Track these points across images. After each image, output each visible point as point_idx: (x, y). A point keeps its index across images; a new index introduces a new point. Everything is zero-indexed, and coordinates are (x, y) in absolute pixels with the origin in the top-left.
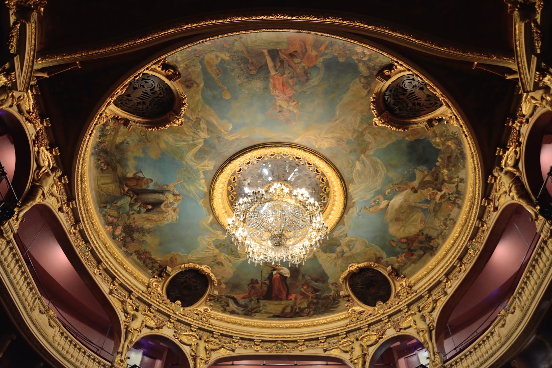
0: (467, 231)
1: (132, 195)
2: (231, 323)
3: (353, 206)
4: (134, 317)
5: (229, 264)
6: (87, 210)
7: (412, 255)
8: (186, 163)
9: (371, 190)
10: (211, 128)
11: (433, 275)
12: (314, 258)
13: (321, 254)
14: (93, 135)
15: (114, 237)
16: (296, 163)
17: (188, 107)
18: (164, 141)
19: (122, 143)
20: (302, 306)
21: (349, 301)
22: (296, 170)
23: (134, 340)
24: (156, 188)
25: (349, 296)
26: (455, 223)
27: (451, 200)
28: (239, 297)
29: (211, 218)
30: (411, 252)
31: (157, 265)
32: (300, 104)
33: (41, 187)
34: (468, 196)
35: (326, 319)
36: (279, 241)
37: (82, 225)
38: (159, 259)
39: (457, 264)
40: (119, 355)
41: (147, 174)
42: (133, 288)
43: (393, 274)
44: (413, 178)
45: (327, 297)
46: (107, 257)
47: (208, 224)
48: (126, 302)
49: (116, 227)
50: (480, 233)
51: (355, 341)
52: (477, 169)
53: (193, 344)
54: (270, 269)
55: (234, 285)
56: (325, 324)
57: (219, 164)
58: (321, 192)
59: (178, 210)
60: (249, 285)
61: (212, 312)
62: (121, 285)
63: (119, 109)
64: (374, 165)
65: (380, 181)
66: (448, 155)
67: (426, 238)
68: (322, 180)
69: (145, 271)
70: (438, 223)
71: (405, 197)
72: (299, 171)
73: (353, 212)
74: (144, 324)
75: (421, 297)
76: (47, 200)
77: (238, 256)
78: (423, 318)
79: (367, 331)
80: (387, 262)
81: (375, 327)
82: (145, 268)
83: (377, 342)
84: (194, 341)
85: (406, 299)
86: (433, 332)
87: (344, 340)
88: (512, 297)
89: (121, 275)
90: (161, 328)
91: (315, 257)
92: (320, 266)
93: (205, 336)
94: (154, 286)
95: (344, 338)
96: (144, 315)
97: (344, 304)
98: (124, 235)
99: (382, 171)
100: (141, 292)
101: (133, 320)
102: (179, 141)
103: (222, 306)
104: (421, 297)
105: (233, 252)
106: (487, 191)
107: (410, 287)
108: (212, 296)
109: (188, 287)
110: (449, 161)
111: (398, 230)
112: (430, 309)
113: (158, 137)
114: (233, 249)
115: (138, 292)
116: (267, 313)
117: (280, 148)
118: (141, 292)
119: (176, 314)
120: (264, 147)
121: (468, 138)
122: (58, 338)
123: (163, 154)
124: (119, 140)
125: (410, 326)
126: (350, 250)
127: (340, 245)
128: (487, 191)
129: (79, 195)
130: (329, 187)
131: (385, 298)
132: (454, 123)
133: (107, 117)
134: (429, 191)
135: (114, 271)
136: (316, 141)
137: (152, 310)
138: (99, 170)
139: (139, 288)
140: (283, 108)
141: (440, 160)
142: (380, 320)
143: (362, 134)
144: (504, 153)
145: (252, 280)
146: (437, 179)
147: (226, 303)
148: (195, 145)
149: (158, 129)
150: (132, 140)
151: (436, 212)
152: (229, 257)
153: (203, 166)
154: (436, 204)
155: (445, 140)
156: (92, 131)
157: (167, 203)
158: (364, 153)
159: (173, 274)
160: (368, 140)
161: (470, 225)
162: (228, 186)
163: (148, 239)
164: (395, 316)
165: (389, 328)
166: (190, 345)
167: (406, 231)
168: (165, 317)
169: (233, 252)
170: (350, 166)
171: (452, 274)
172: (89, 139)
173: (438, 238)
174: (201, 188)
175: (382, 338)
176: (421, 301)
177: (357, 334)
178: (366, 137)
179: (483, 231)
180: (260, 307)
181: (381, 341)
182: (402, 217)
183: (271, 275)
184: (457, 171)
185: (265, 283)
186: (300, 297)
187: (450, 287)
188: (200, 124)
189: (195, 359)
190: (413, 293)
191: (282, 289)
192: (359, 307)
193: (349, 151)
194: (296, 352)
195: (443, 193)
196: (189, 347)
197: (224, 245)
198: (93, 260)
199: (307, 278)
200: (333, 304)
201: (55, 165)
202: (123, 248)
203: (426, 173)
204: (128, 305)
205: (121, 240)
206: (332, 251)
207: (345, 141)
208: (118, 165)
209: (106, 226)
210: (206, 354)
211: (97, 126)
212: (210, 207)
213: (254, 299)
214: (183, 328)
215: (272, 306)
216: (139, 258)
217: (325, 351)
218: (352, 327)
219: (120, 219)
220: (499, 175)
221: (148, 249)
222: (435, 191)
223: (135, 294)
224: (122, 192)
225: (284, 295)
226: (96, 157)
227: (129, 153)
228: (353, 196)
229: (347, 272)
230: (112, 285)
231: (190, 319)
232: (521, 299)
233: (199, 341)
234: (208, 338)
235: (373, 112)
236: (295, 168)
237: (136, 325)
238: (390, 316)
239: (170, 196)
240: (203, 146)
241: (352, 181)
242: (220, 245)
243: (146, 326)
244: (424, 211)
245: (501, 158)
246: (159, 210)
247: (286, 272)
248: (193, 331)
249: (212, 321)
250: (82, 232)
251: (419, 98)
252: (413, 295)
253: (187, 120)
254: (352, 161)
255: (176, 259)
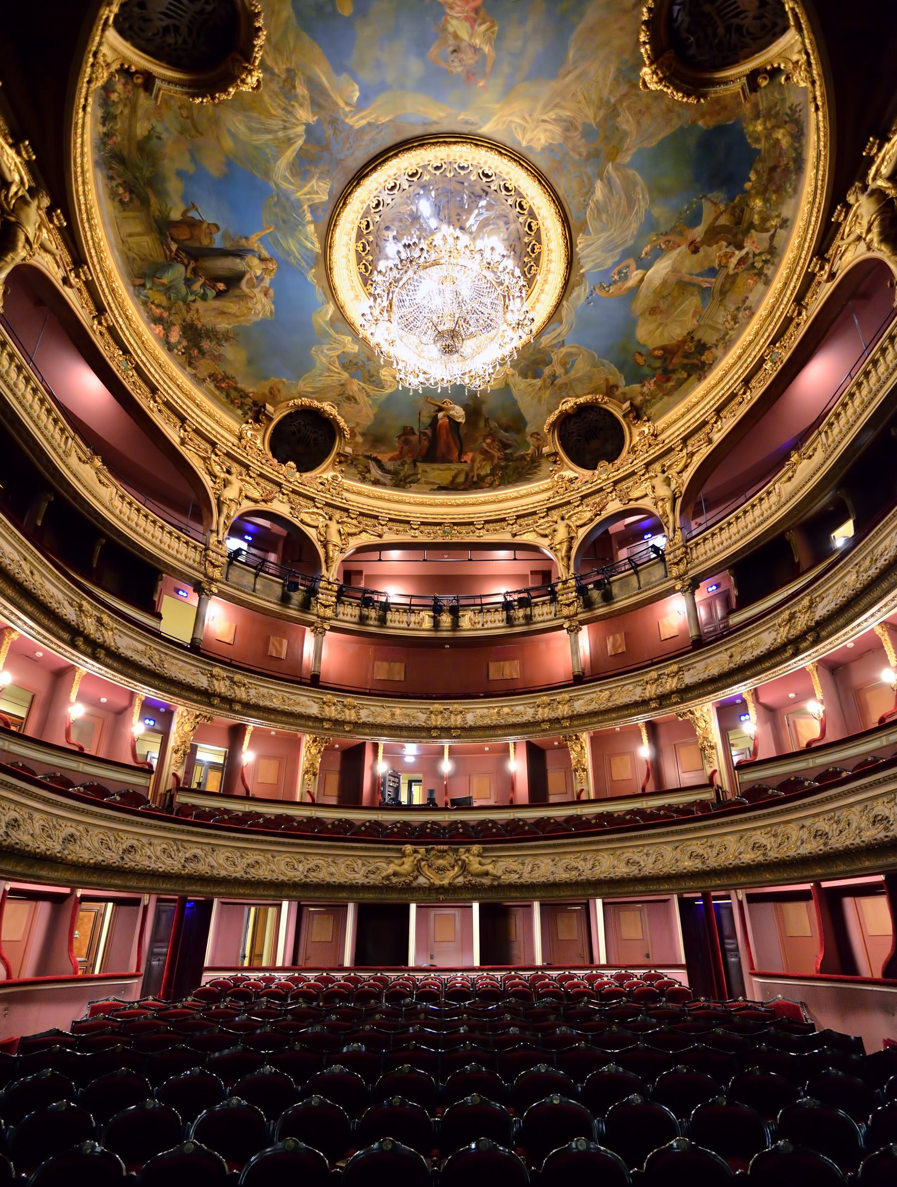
0: (771, 327)
1: (186, 261)
2: (375, 498)
3: (579, 284)
4: (226, 483)
5: (366, 398)
6: (113, 290)
7: (668, 380)
8: (276, 185)
9: (616, 247)
10: (319, 99)
11: (693, 416)
12: (506, 389)
13: (518, 379)
14: (89, 109)
15: (170, 347)
16: (483, 188)
17: (268, 39)
18: (229, 131)
19: (148, 138)
20: (483, 473)
21: (555, 462)
22: (483, 203)
23: (232, 514)
24: (227, 245)
25: (556, 454)
26: (753, 314)
27: (755, 268)
28: (384, 458)
29: (331, 309)
30: (667, 374)
31: (249, 401)
32: (496, 28)
33: (18, 224)
34: (789, 256)
35: (518, 491)
36: (450, 341)
37: (109, 315)
38: (251, 390)
39: (739, 390)
40: (214, 535)
41: (207, 214)
42: (216, 437)
43: (631, 415)
44: (695, 219)
45: (523, 458)
46: (164, 382)
47: (326, 322)
48: (209, 458)
49: (169, 327)
50: (792, 328)
51: (559, 521)
52: (819, 192)
53: (320, 525)
54: (433, 409)
55: (375, 438)
56: (516, 498)
57: (338, 188)
58: (527, 251)
59: (271, 292)
60: (399, 437)
61: (344, 480)
62: (197, 431)
63: (128, 45)
64: (629, 187)
65: (634, 226)
66: (771, 165)
67: (696, 347)
68: (530, 227)
69: (231, 411)
70: (722, 317)
71: (674, 262)
72: (489, 207)
73: (580, 293)
74: (243, 494)
75: (670, 450)
76: (36, 257)
77: (379, 384)
78: (668, 481)
79: (578, 506)
80: (624, 394)
81: (590, 500)
82: (231, 407)
83: (591, 520)
84: (321, 522)
85: (646, 455)
86: (679, 502)
87: (542, 521)
88: (817, 431)
89: (193, 415)
90: (271, 500)
91: (507, 385)
92: (515, 403)
93: (337, 515)
94: (249, 435)
95: (543, 518)
96: (242, 480)
97: (547, 466)
98: (185, 343)
99: (642, 203)
100: (230, 445)
101: (225, 487)
102: (258, 131)
103: (360, 473)
104: (670, 450)
105: (372, 376)
106: (828, 232)
107: (656, 436)
108: (342, 455)
109: (304, 439)
110: (770, 180)
111: (651, 333)
112: (678, 469)
113: (215, 122)
114: (372, 372)
115: (226, 445)
116: (428, 483)
117: (454, 147)
118: (230, 445)
119: (290, 482)
120: (422, 145)
121: (820, 114)
122: (117, 502)
123: (229, 163)
124: (141, 129)
125: (646, 495)
126: (567, 372)
127: (550, 362)
128: (828, 232)
129: (90, 252)
130: (540, 243)
131: (612, 457)
132: (800, 79)
133: (108, 65)
134: (720, 249)
135: (181, 407)
136: (524, 130)
137: (252, 474)
138: (117, 204)
139: (226, 441)
140: (462, 40)
141: (753, 177)
142: (601, 490)
143: (614, 112)
144: (879, 150)
145: (405, 428)
146: (738, 222)
147: (366, 467)
148: (289, 141)
149: (213, 98)
150: (167, 128)
151: (723, 293)
152: (365, 386)
153: (309, 193)
154: (728, 276)
155: (774, 127)
156: (86, 100)
157: (252, 278)
158: (613, 160)
159: (277, 418)
160: (625, 127)
161: (779, 313)
162: (357, 242)
163: (229, 351)
164: (624, 483)
165: (613, 500)
166: (316, 527)
167: (666, 334)
168: (274, 486)
169: (372, 376)
170: (584, 190)
171: (727, 409)
172: (84, 118)
173: (716, 346)
174: (309, 245)
175: (600, 515)
176: (669, 456)
177: (563, 511)
178: (620, 119)
179: (798, 325)
180: (417, 474)
181: (598, 519)
182: (663, 305)
183: (435, 419)
184: (780, 203)
185: (425, 434)
186: (480, 457)
187: (719, 430)
188: (294, 87)
189: (325, 545)
190: (657, 445)
191: (453, 445)
192: (570, 471)
193: (585, 154)
194: (472, 538)
195: (744, 252)
196: (314, 530)
197: (356, 364)
198: (143, 385)
199: (493, 424)
200: (530, 469)
201: (33, 184)
202: (188, 368)
203: (722, 207)
204: (213, 463)
205: (183, 354)
206: (537, 375)
207: (580, 128)
208: (149, 190)
209: (152, 325)
210: (341, 540)
211: (93, 86)
212: (326, 285)
213: (408, 461)
214: (302, 503)
215: (437, 473)
216: (218, 388)
217: (514, 535)
218: (557, 500)
219: (173, 311)
220: (857, 200)
221: (230, 372)
222: (731, 249)
223: (222, 447)
224: (168, 253)
225: (456, 454)
226: (105, 172)
227: (166, 163)
228: (582, 261)
229: (557, 412)
230: (182, 431)
231: (311, 490)
232: (829, 433)
233: (329, 522)
234: (341, 517)
235: (643, 50)
236: (480, 197)
237: (231, 493)
238: (616, 483)
239: (255, 262)
240: (305, 142)
241: (583, 228)
242: (349, 364)
243: (247, 497)
244: (705, 292)
245: (871, 161)
246: (237, 292)
247: (458, 413)
248: (318, 508)
249: (346, 495)
250: (112, 330)
251: (742, 12)
252: (657, 448)
253: (268, 77)
254: (589, 179)
255: (279, 391)
